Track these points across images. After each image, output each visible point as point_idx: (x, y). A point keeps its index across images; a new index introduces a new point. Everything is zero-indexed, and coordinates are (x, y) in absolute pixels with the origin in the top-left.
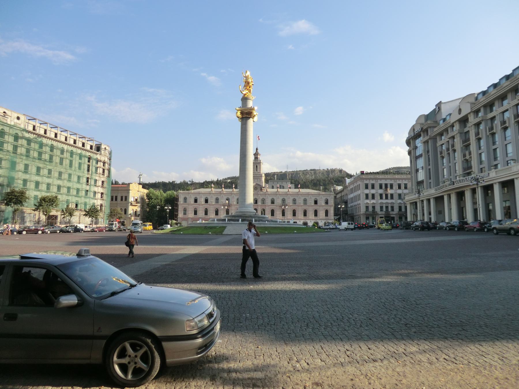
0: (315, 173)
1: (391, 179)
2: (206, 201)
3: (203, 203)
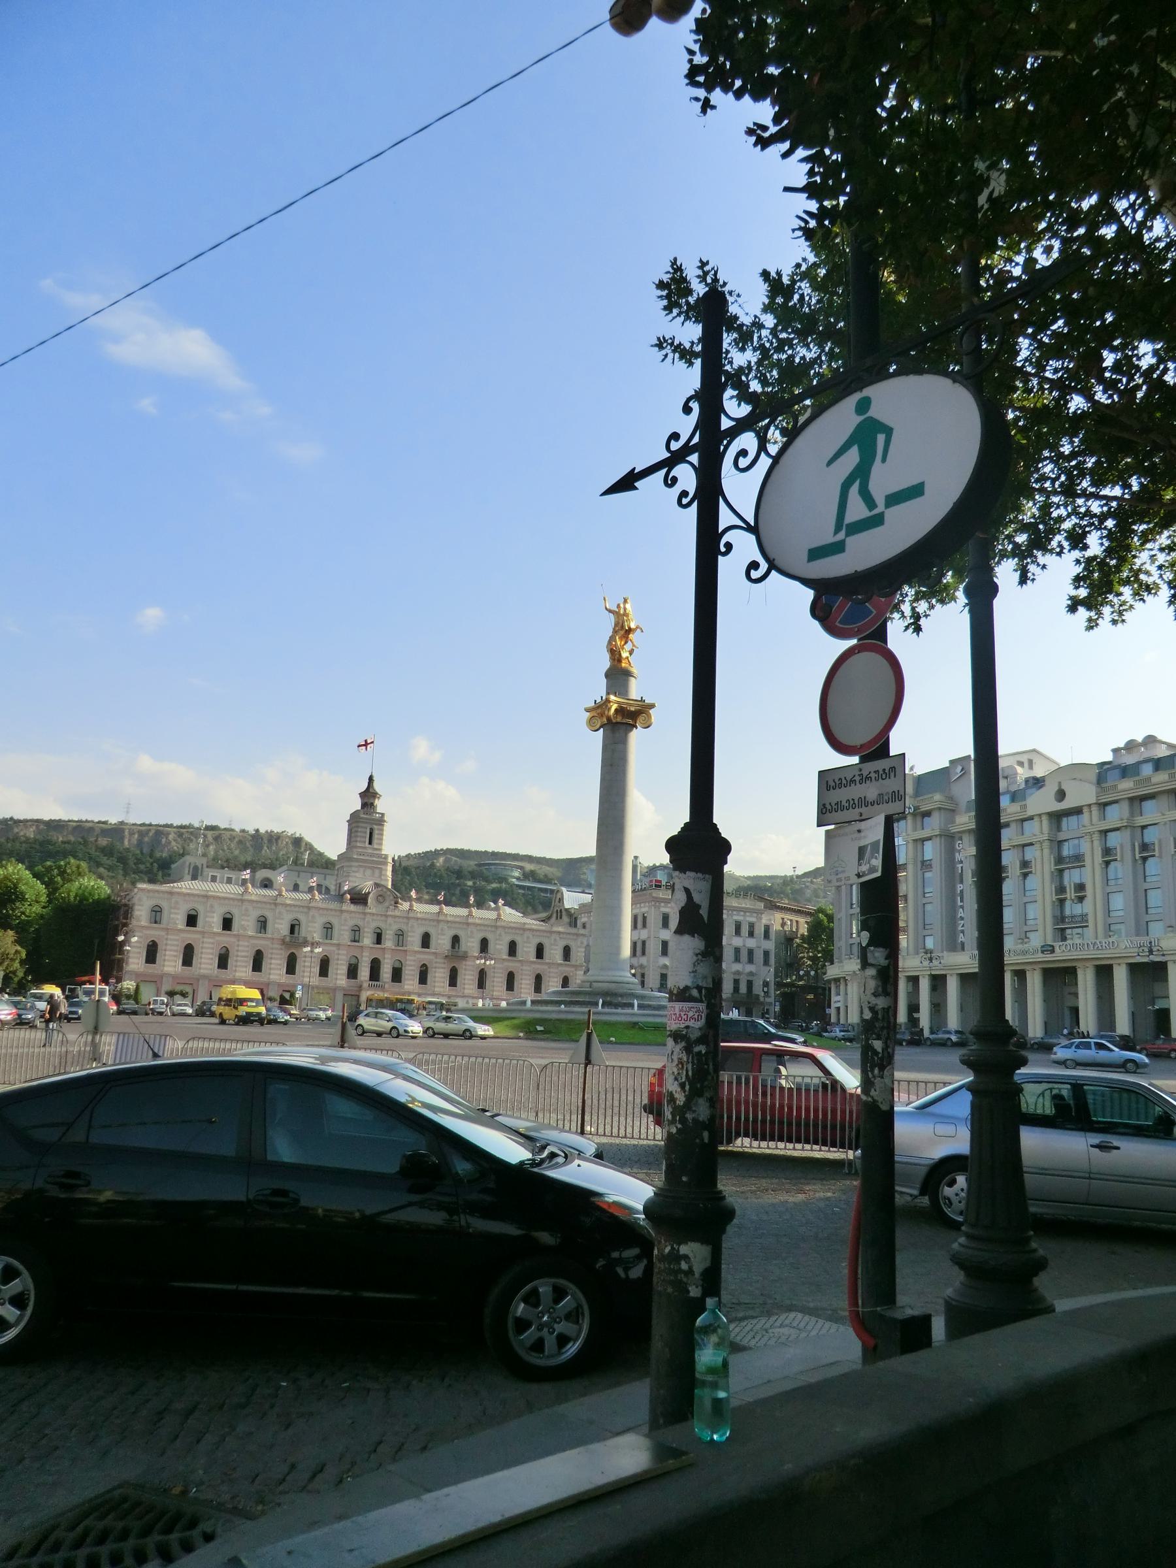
0: (217, 839)
2: (227, 924)
3: (217, 927)
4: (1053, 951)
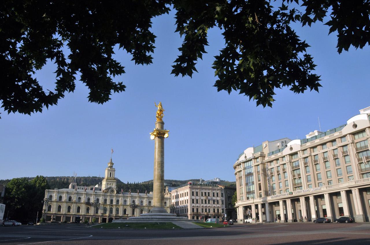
4: (292, 194)
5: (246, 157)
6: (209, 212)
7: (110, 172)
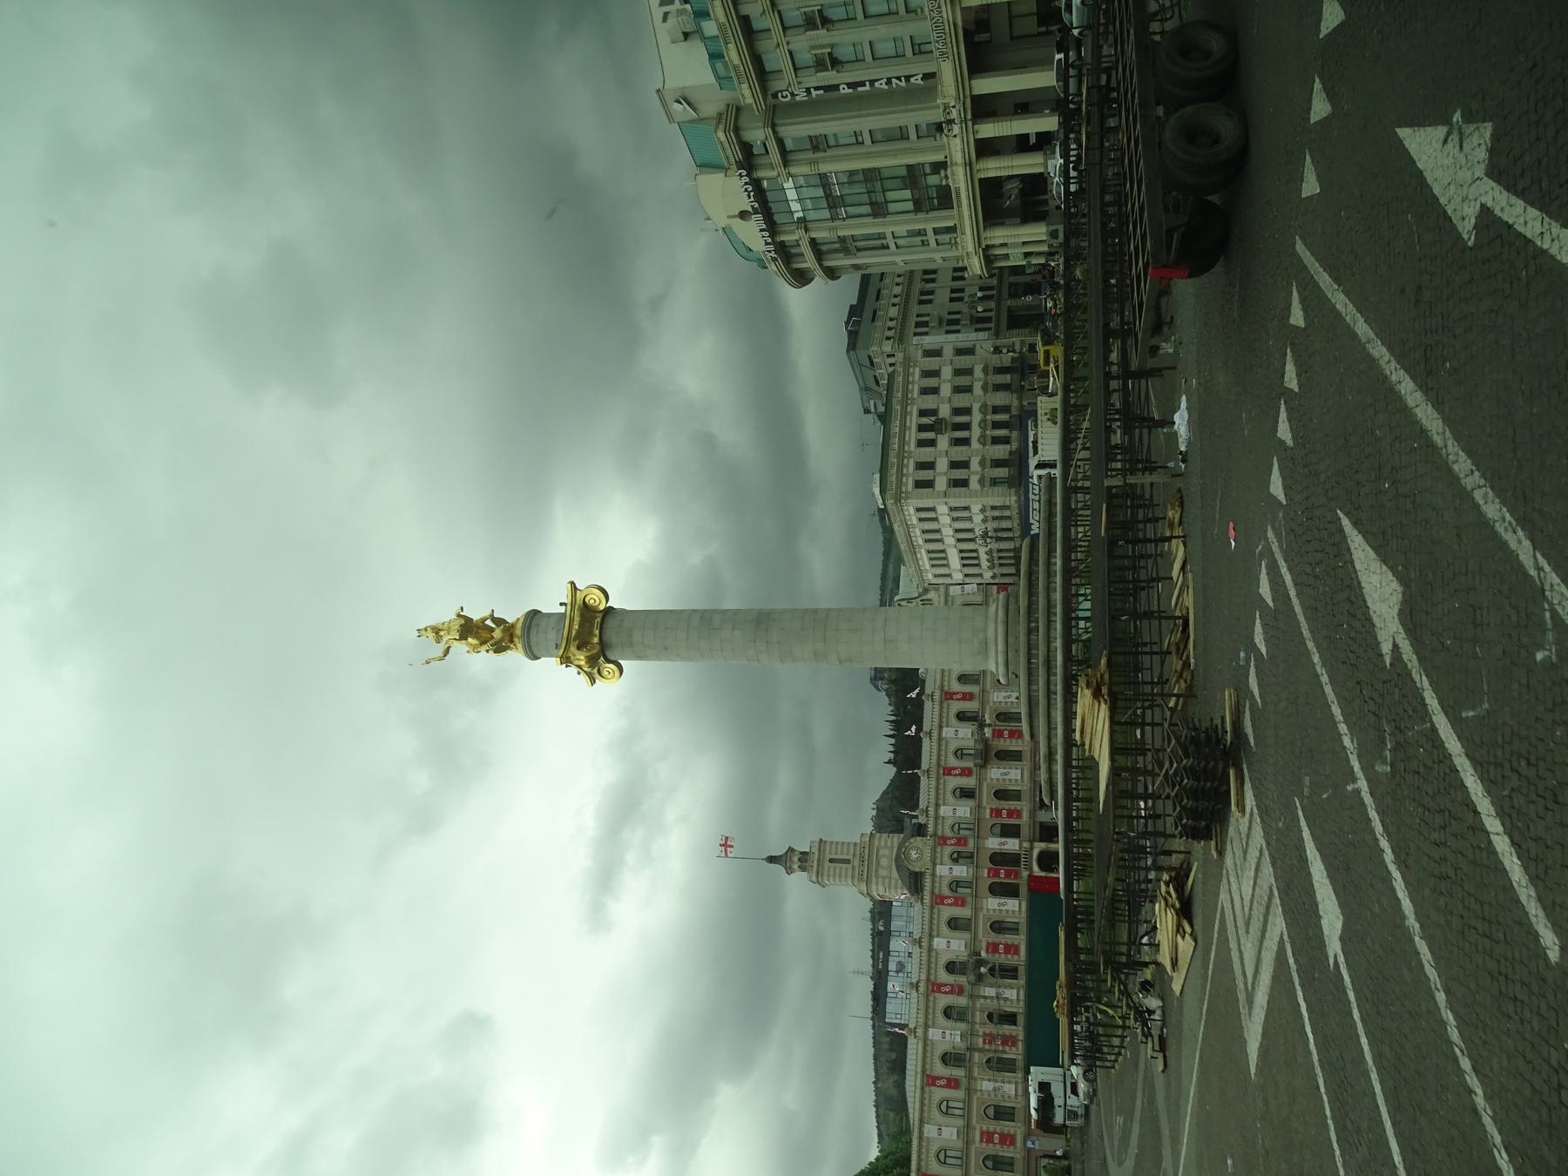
1: (905, 414)
5: (743, 215)
6: (1006, 409)
7: (827, 864)
